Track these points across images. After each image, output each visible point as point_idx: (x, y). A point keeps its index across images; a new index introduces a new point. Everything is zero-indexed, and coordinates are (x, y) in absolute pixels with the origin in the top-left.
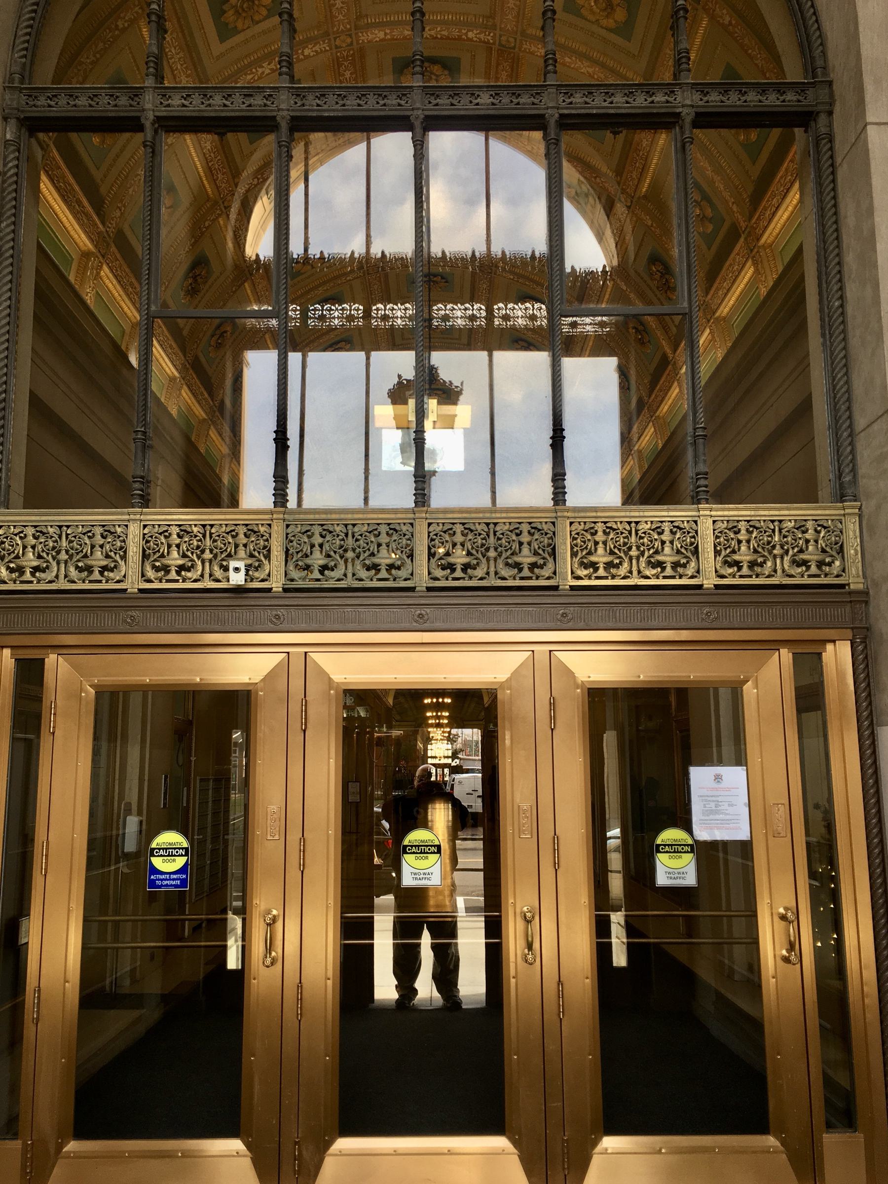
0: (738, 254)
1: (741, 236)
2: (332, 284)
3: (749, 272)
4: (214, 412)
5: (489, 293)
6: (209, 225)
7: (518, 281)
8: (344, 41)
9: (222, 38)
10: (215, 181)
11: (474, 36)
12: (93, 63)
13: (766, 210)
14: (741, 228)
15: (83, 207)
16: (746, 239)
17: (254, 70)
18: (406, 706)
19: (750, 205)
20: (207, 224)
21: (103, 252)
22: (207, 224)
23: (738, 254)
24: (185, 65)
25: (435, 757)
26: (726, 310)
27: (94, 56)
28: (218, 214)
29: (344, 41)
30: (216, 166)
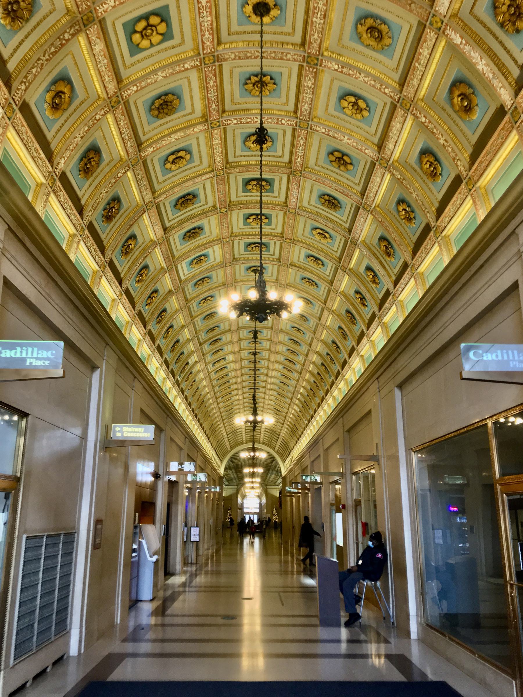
0: (430, 239)
1: (462, 181)
2: (171, 71)
3: (468, 203)
4: (84, 230)
5: (305, 150)
6: (121, 176)
7: (342, 72)
8: (215, 124)
9: (132, 55)
10: (103, 81)
11: (291, 57)
12: (47, 60)
13: (482, 163)
14: (463, 175)
15: (39, 154)
16: (411, 268)
17: (152, 77)
18: (232, 476)
19: (515, 86)
20: (119, 175)
21: (81, 234)
22: (119, 175)
23: (502, 129)
24: (108, 69)
25: (249, 508)
26: (424, 268)
27: (49, 56)
28: (77, 30)
29: (215, 124)
30: (127, 138)
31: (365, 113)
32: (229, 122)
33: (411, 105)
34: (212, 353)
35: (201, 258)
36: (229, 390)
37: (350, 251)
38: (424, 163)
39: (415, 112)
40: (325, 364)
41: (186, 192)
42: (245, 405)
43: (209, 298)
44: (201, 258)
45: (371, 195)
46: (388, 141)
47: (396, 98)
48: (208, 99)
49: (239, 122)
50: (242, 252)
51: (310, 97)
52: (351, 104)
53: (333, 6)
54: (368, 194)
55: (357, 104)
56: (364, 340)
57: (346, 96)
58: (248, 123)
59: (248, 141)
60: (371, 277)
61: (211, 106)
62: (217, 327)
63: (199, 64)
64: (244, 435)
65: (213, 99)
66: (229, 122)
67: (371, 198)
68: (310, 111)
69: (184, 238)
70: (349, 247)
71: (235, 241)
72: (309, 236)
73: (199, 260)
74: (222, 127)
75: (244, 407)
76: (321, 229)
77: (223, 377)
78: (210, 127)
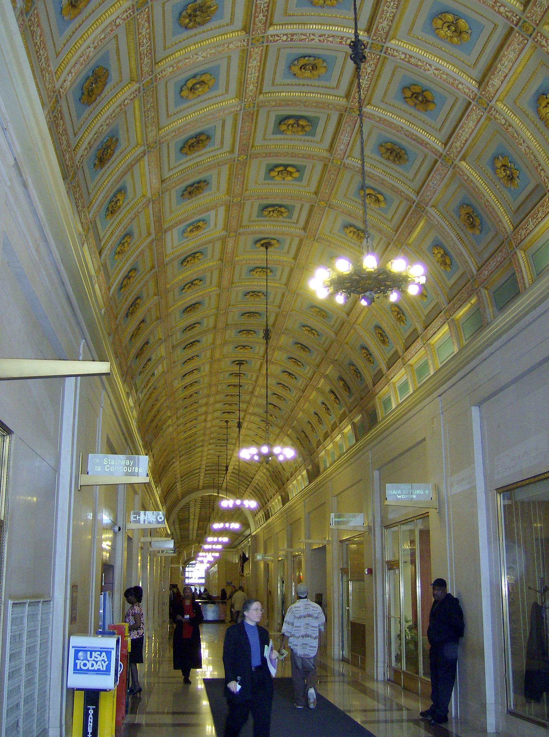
31: (383, 205)
32: (277, 38)
33: (534, 29)
34: (183, 345)
35: (199, 224)
36: (195, 414)
37: (413, 220)
38: (543, 105)
39: (539, 38)
40: (336, 392)
41: (199, 130)
42: (212, 436)
43: (197, 282)
44: (199, 224)
45: (458, 144)
46: (494, 74)
47: (515, 19)
48: (256, 6)
49: (289, 39)
50: (254, 217)
51: (393, 12)
52: (446, 24)
53: (336, 193)
54: (452, 144)
55: (456, 24)
56: (418, 344)
57: (441, 13)
58: (301, 40)
59: (294, 65)
60: (439, 255)
61: (258, 17)
62: (198, 323)
63: (246, 45)
64: (202, 478)
65: (262, 7)
66: (277, 38)
67: (456, 148)
68: (389, 30)
69: (183, 195)
70: (412, 214)
71: (247, 202)
72: (353, 198)
73: (196, 227)
74: (265, 44)
75: (211, 439)
76: (373, 189)
77: (191, 396)
78: (250, 44)
